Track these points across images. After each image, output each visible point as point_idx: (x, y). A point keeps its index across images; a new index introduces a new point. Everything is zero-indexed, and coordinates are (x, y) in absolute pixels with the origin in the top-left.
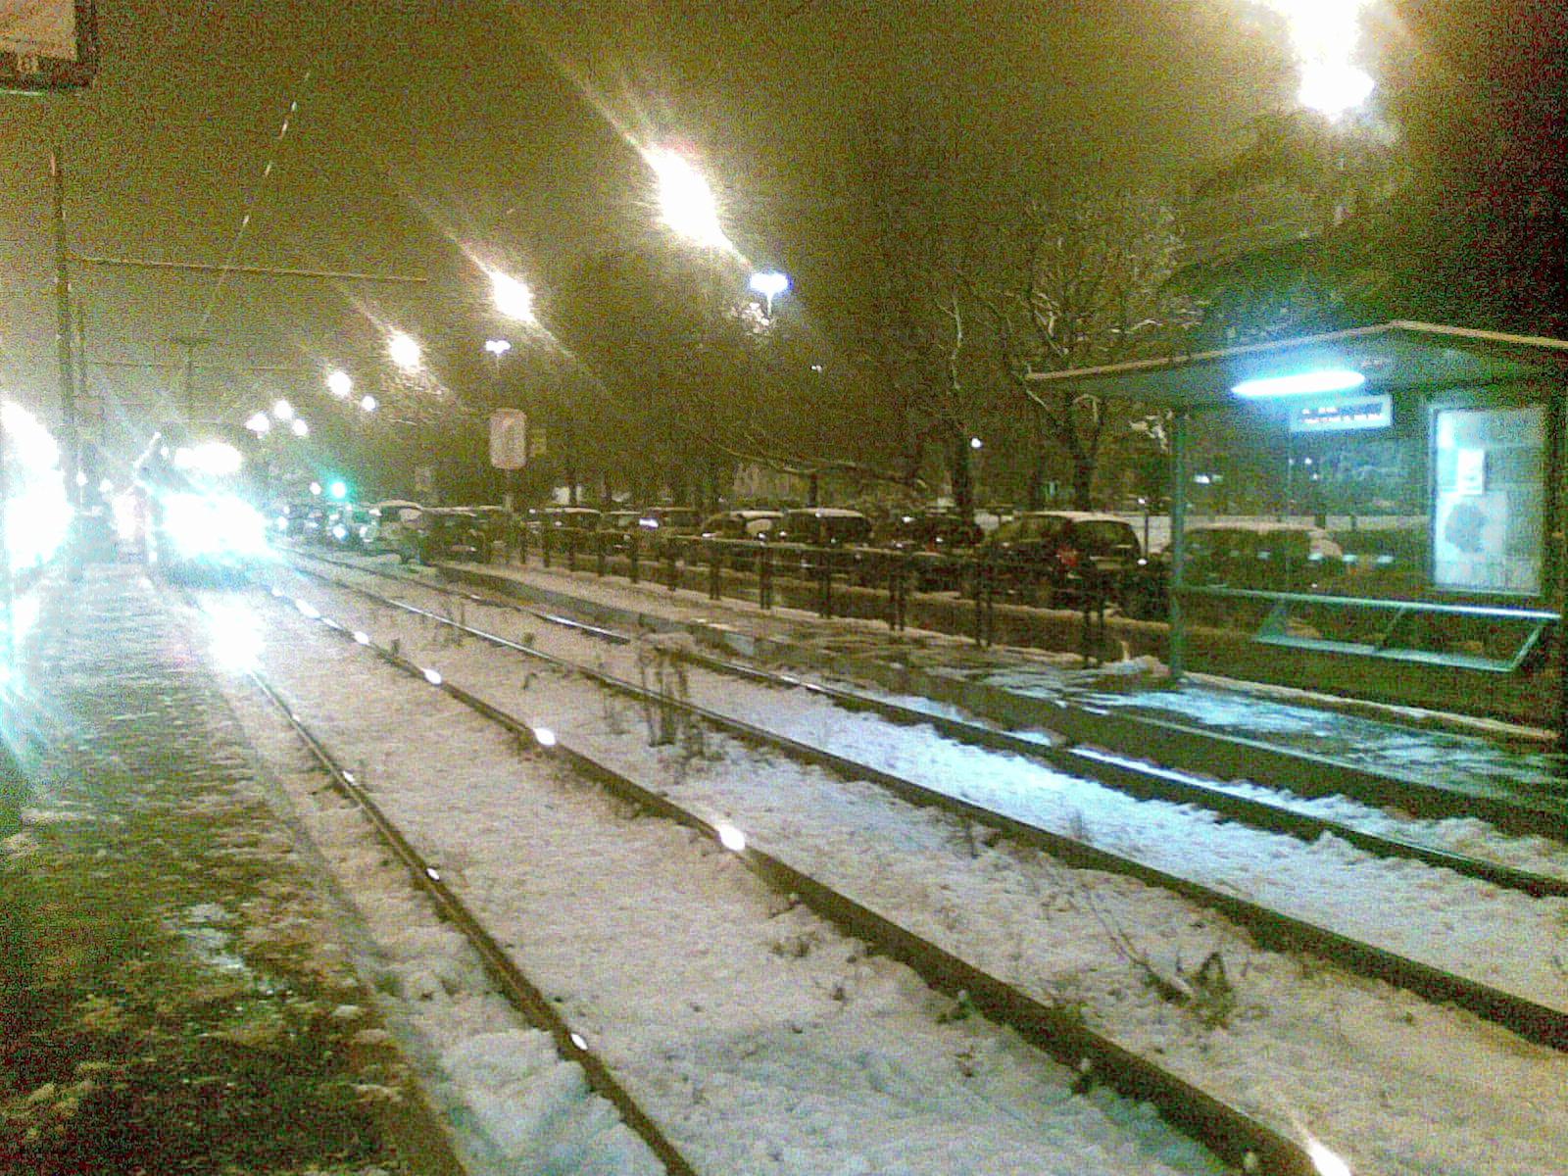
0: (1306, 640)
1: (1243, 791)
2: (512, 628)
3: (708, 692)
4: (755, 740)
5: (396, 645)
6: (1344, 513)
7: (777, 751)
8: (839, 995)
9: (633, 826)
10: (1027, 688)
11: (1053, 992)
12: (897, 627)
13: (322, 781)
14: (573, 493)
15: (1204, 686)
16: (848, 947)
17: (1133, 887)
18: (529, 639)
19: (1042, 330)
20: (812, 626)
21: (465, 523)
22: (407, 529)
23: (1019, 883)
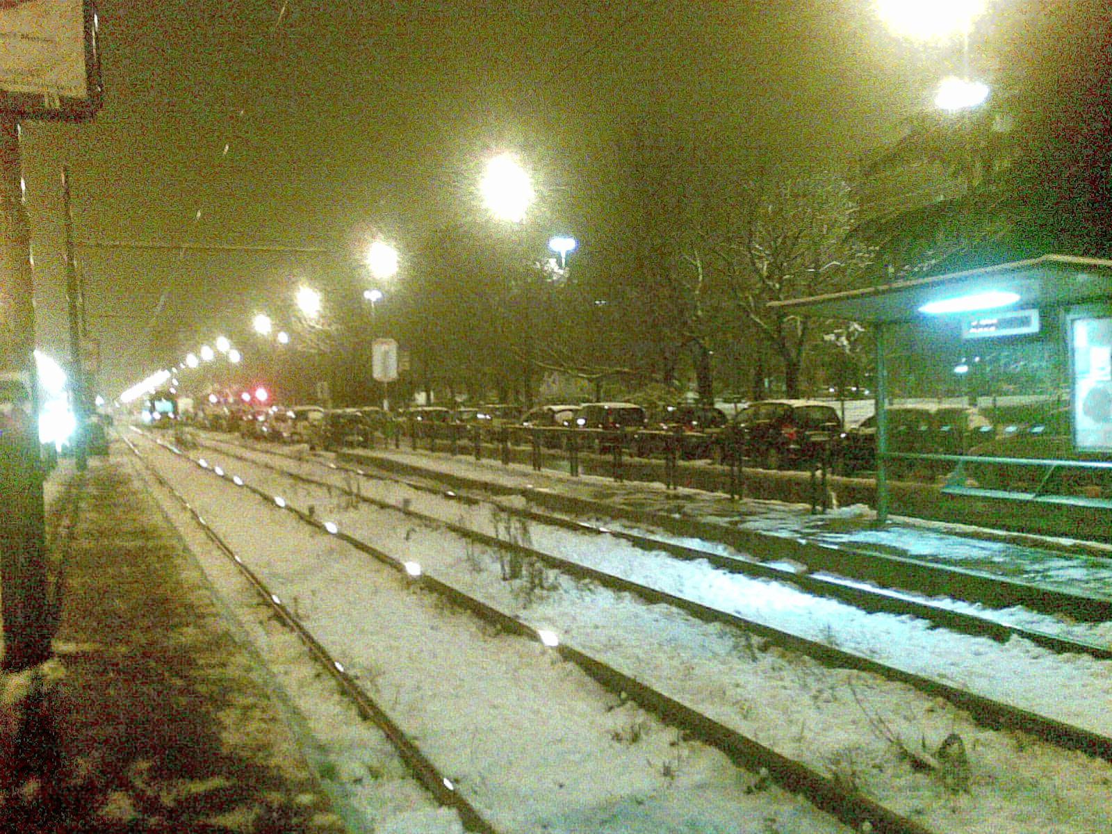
0: (971, 489)
1: (945, 604)
2: (396, 493)
3: (544, 539)
4: (578, 573)
5: (312, 510)
6: (988, 394)
7: (596, 582)
8: (667, 772)
9: (496, 641)
10: (776, 530)
11: (834, 768)
12: (671, 487)
13: (265, 613)
14: (428, 396)
15: (906, 526)
16: (671, 733)
17: (878, 681)
18: (407, 502)
19: (757, 271)
20: (609, 487)
21: (354, 420)
22: (314, 426)
23: (793, 681)
